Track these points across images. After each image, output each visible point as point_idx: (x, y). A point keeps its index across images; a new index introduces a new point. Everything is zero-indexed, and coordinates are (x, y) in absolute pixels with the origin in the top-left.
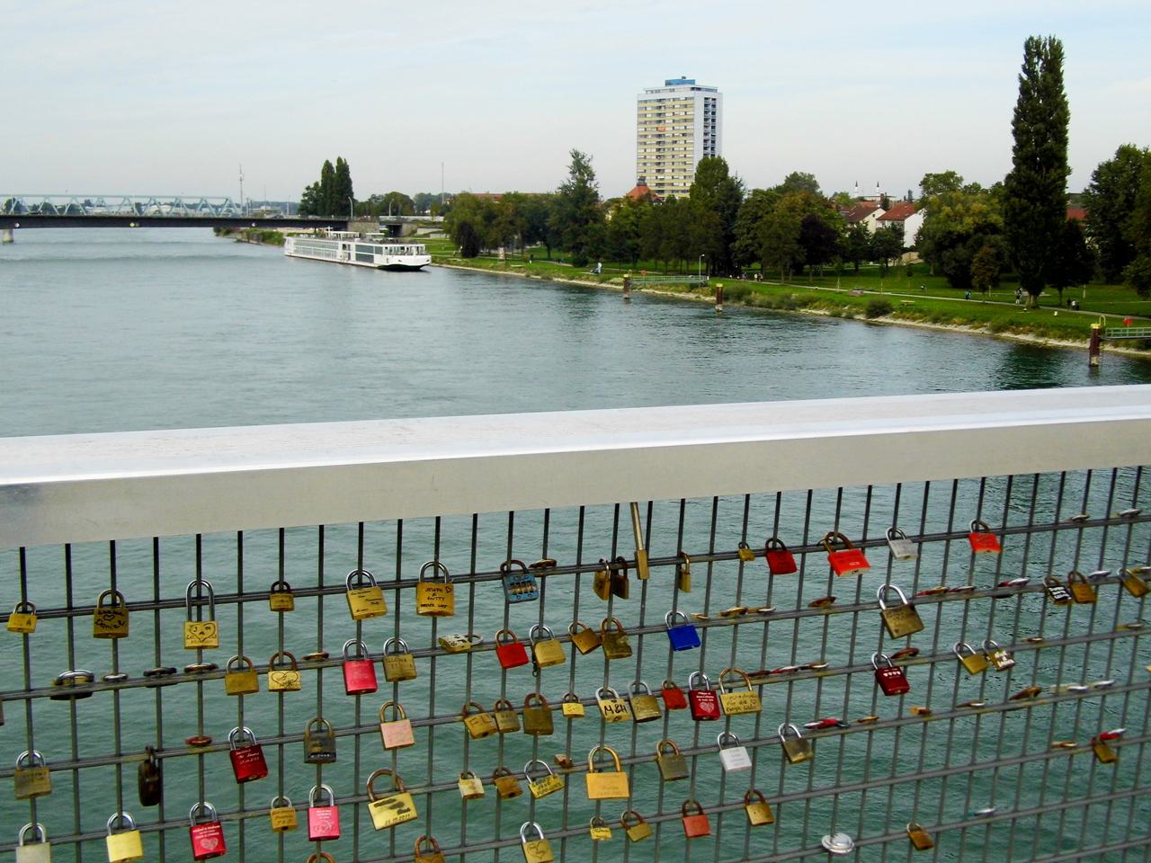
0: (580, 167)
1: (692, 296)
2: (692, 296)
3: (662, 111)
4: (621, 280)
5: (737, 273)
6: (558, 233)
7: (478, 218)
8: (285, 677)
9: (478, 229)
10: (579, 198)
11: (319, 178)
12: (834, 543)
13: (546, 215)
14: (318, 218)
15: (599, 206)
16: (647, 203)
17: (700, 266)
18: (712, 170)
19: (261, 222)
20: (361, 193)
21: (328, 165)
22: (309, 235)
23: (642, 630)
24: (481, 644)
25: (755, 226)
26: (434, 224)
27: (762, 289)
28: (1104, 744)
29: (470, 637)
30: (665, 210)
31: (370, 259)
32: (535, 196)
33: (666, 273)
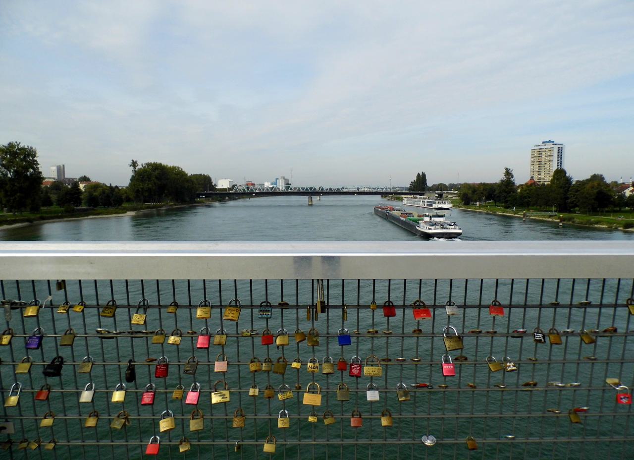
0: (508, 173)
1: (550, 220)
2: (550, 220)
3: (541, 153)
4: (522, 213)
5: (570, 212)
6: (499, 197)
7: (470, 192)
8: (175, 339)
9: (470, 195)
10: (508, 184)
11: (415, 179)
12: (419, 305)
13: (495, 190)
14: (415, 192)
15: (515, 187)
16: (533, 186)
17: (554, 209)
18: (560, 173)
19: (396, 193)
20: (430, 183)
21: (419, 174)
22: (411, 198)
23: (328, 336)
24: (257, 334)
25: (576, 194)
26: (454, 194)
27: (579, 218)
28: (576, 413)
29: (252, 331)
30: (540, 188)
31: (432, 206)
32: (491, 184)
33: (541, 211)
